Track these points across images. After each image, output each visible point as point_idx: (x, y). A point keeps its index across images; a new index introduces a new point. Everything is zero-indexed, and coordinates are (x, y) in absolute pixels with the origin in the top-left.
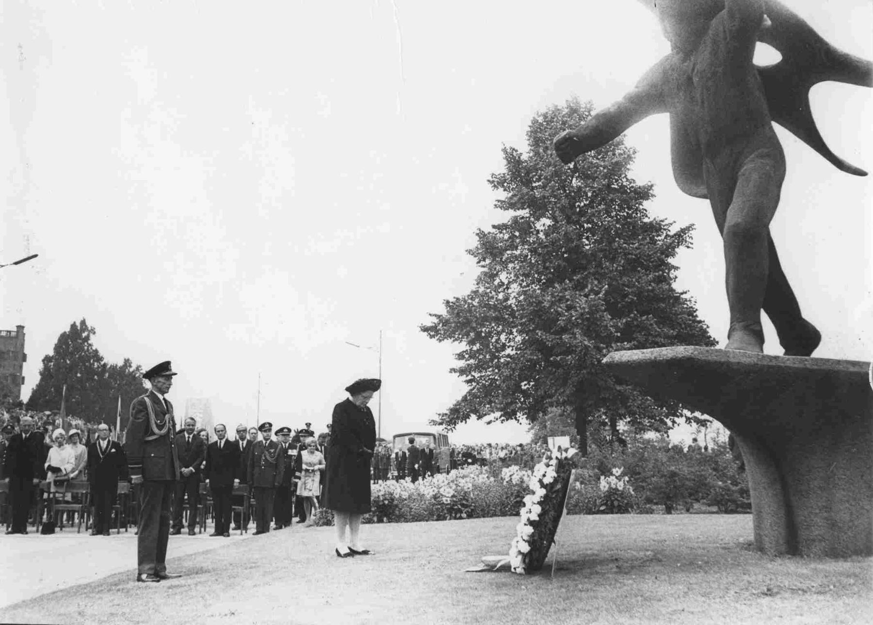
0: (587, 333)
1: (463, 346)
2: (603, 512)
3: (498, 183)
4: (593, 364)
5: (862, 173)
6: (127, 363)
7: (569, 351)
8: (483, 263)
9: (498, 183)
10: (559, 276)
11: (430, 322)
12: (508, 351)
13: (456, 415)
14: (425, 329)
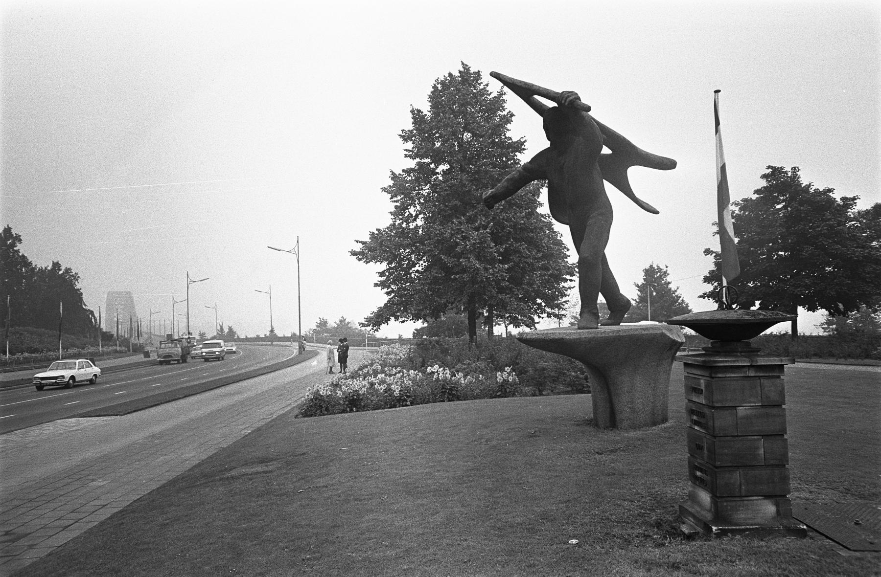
0: (478, 258)
1: (384, 266)
2: (499, 396)
3: (406, 137)
4: (482, 281)
5: (657, 212)
6: (56, 265)
7: (464, 271)
8: (395, 199)
9: (406, 137)
10: (457, 211)
11: (358, 247)
12: (417, 268)
13: (379, 318)
14: (354, 253)
